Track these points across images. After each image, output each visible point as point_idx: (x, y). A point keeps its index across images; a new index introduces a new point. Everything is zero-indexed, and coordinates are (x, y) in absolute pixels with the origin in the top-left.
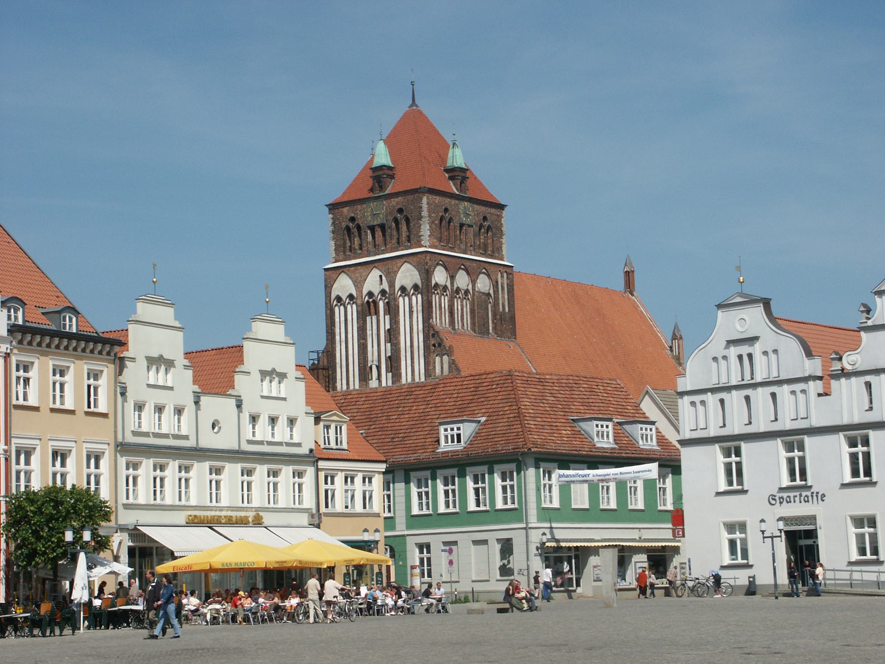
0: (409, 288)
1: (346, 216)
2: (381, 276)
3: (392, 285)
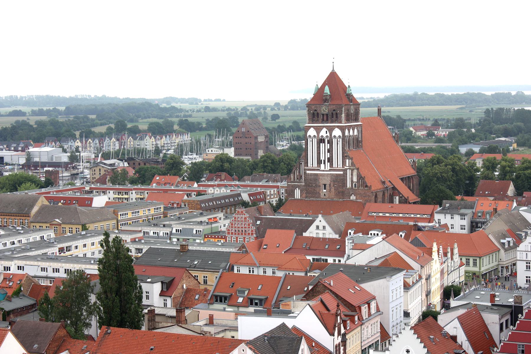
0: (312, 136)
2: (326, 131)
3: (331, 135)
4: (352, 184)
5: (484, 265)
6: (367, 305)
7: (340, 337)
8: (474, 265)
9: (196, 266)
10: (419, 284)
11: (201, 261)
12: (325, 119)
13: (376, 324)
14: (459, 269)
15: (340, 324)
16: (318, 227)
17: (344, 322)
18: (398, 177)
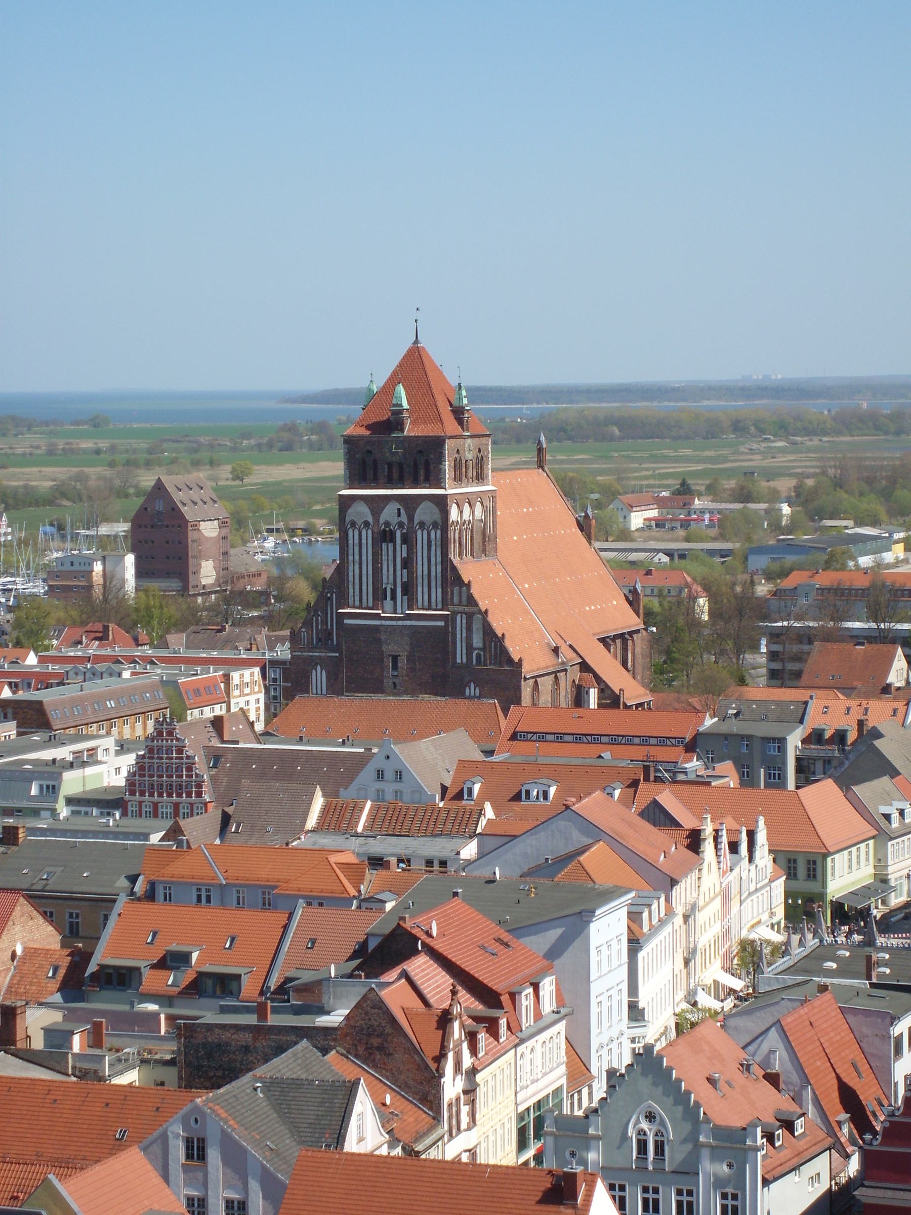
2: (399, 510)
3: (411, 518)
4: (469, 655)
5: (837, 874)
6: (530, 990)
7: (459, 1078)
8: (809, 876)
9: (47, 885)
10: (668, 929)
11: (62, 871)
12: (395, 475)
13: (555, 1040)
14: (768, 888)
15: (459, 1044)
16: (380, 775)
17: (472, 1037)
18: (594, 635)
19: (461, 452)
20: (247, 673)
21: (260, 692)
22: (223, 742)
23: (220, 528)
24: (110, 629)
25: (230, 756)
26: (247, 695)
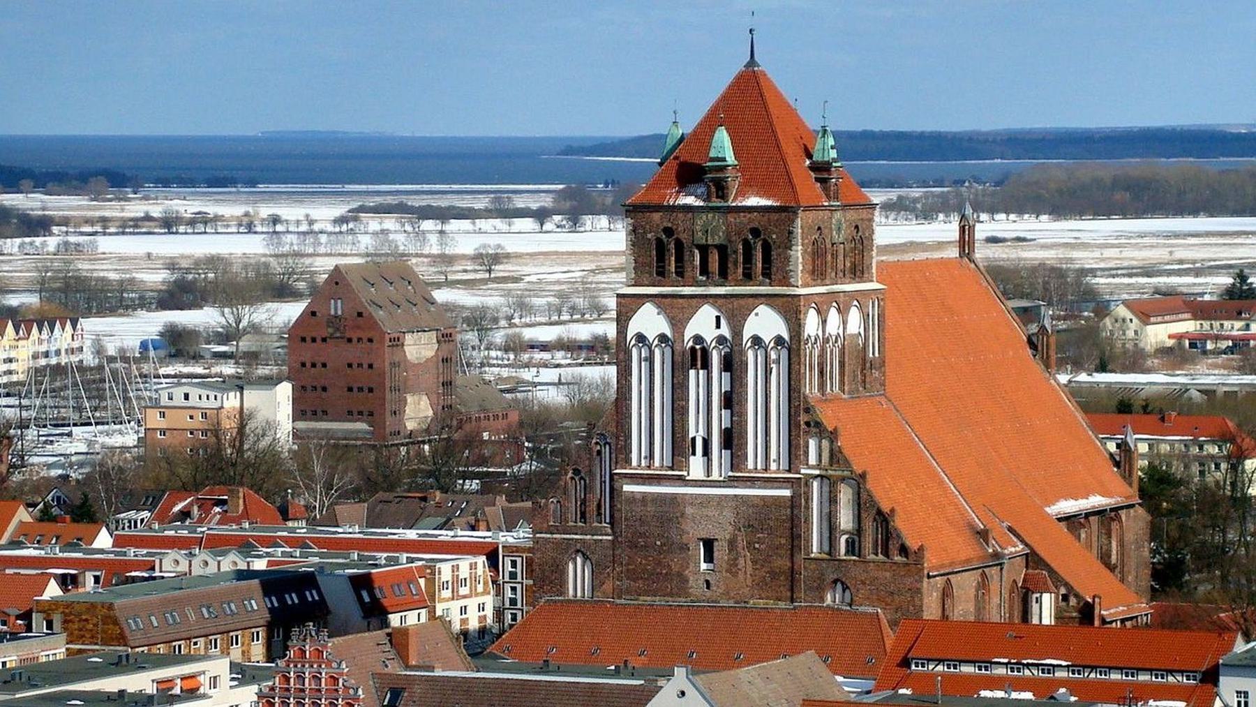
1: (658, 225)
2: (718, 318)
3: (737, 332)
19: (825, 231)
20: (464, 564)
21: (486, 592)
22: (408, 667)
23: (438, 342)
24: (241, 495)
25: (417, 689)
26: (465, 597)
